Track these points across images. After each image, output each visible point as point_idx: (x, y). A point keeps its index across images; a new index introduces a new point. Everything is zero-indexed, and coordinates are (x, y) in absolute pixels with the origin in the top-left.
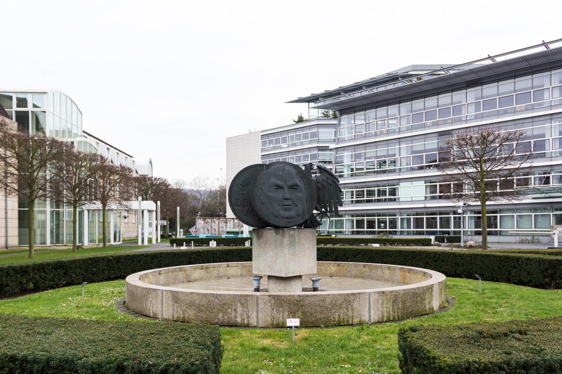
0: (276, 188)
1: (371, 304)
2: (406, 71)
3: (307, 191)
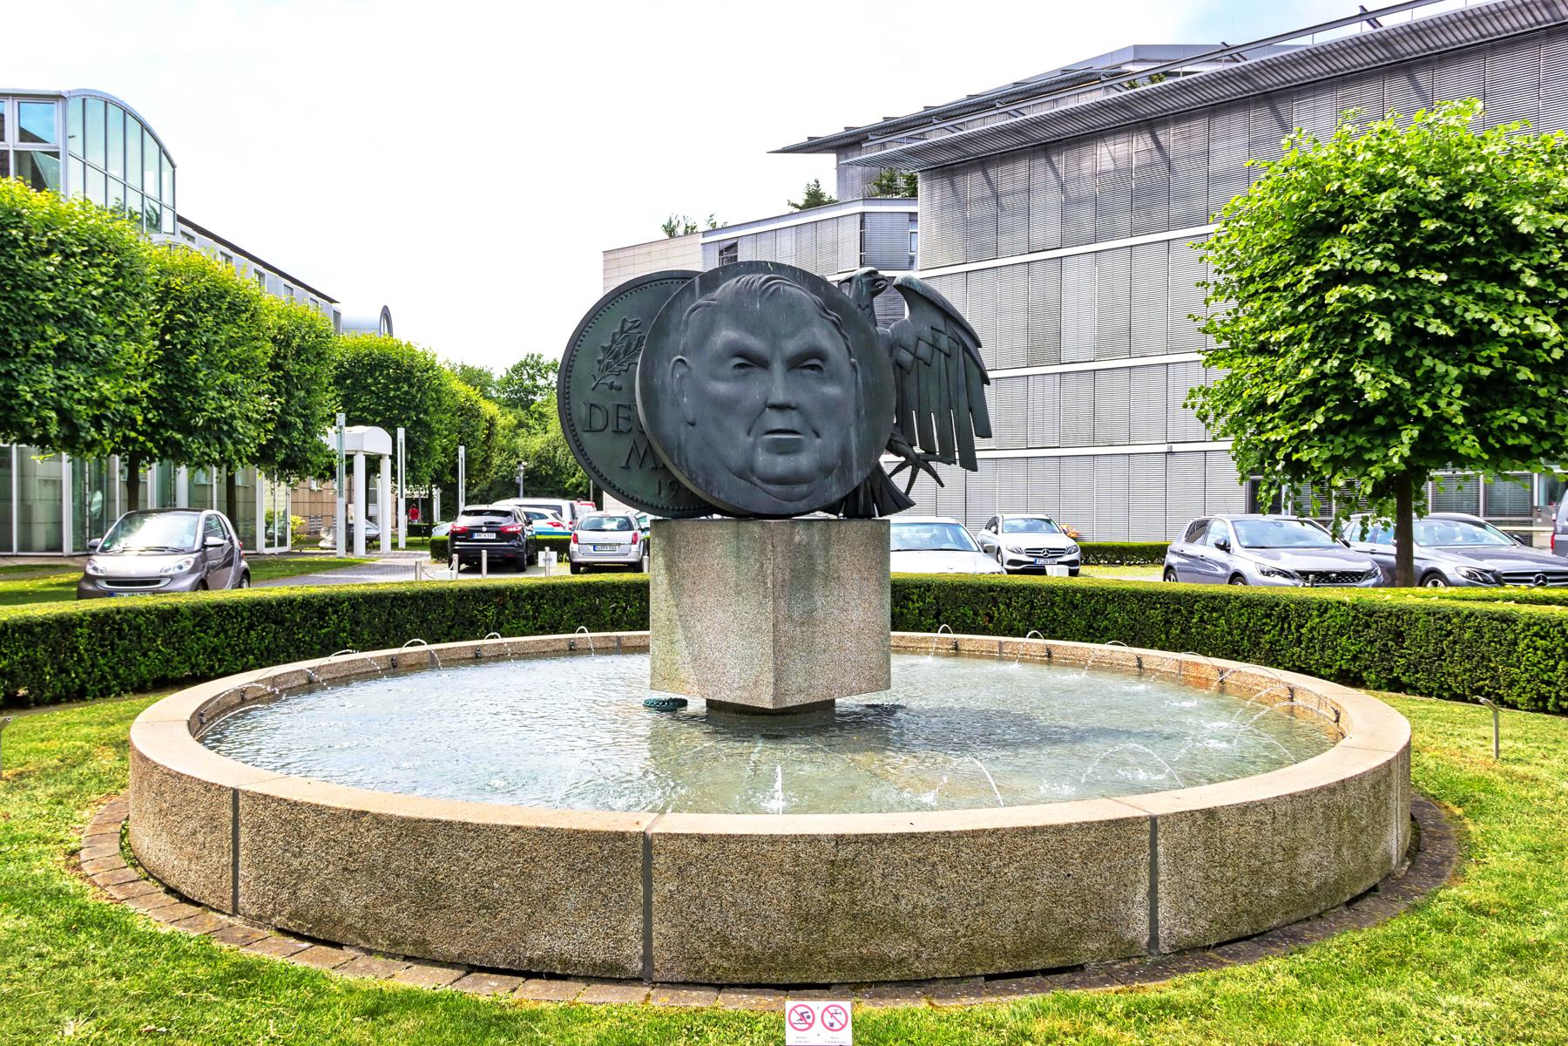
0: (740, 366)
1: (1162, 868)
2: (1116, 62)
3: (860, 380)
